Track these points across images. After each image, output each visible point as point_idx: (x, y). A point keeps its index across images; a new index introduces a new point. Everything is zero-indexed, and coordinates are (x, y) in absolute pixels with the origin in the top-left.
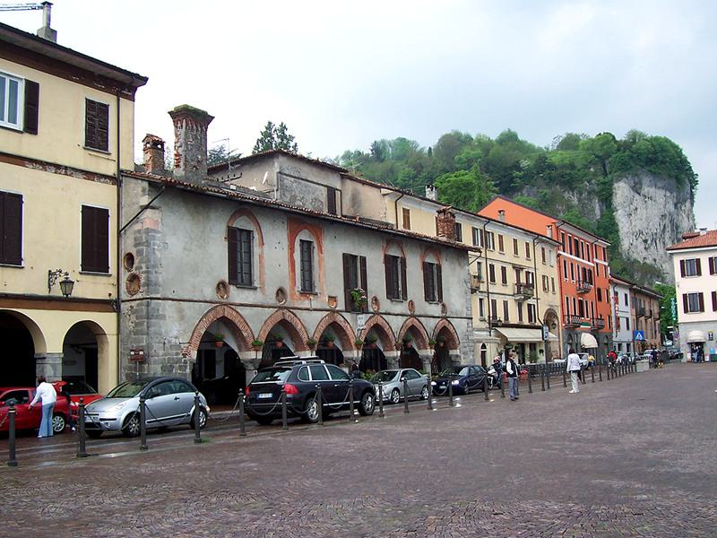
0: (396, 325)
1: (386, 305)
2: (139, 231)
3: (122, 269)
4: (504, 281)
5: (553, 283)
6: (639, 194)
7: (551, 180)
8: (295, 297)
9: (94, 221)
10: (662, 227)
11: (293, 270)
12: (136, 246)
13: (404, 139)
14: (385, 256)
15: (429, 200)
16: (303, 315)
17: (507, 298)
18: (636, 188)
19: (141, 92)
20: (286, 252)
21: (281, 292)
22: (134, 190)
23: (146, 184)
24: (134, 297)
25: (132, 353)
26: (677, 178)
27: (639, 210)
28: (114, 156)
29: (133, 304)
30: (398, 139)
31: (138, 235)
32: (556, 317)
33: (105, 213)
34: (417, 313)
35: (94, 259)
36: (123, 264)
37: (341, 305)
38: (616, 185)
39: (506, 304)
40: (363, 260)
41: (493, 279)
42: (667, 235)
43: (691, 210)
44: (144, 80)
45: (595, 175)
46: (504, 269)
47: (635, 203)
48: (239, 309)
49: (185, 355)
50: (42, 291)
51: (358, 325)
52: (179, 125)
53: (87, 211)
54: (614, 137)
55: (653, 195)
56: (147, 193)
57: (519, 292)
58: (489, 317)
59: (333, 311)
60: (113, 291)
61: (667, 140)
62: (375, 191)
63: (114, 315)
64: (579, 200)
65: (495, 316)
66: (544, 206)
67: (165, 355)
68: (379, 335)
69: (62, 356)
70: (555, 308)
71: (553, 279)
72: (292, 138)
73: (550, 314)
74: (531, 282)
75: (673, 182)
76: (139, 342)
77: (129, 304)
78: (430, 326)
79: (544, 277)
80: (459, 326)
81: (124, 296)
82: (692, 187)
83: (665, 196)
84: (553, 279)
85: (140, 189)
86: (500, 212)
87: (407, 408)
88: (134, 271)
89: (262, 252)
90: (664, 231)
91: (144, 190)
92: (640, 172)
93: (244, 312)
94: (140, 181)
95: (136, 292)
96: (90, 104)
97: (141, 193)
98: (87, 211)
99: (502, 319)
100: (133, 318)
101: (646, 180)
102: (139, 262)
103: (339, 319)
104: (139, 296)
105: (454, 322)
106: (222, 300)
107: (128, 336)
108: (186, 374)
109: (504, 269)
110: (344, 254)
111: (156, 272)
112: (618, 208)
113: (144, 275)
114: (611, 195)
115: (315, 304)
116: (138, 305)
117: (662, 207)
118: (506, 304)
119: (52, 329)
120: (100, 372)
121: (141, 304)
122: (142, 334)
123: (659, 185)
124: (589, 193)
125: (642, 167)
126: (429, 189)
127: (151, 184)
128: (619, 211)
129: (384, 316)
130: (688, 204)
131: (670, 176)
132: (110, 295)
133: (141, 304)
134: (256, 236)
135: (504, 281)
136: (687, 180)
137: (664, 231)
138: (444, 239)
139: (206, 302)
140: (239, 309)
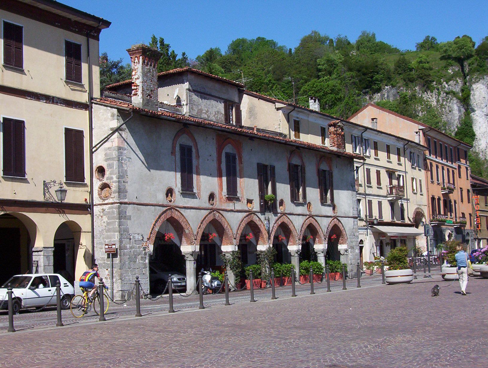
0: (297, 224)
1: (289, 207)
3: (94, 179)
4: (379, 183)
5: (421, 185)
7: (409, 81)
8: (223, 200)
9: (74, 139)
12: (106, 160)
13: (263, 38)
14: (290, 165)
15: (312, 111)
16: (187, 213)
17: (381, 199)
19: (104, 33)
21: (212, 197)
23: (115, 111)
24: (106, 202)
25: (107, 247)
28: (87, 87)
29: (104, 207)
30: (259, 39)
31: (108, 152)
32: (423, 215)
33: (81, 132)
34: (313, 213)
35: (74, 172)
36: (95, 174)
37: (256, 206)
39: (380, 203)
40: (273, 168)
41: (369, 181)
44: (107, 24)
46: (378, 173)
48: (182, 211)
49: (145, 249)
50: (40, 198)
51: (268, 222)
52: (136, 61)
53: (68, 132)
54: (470, 38)
56: (116, 117)
57: (391, 193)
58: (366, 216)
59: (251, 213)
60: (87, 196)
62: (270, 104)
63: (89, 215)
64: (438, 101)
65: (371, 215)
66: (403, 109)
67: (131, 248)
68: (284, 232)
69: (53, 249)
70: (422, 207)
71: (420, 181)
72: (168, 46)
73: (419, 215)
74: (401, 185)
76: (111, 238)
77: (100, 208)
78: (324, 225)
79: (413, 179)
80: (347, 225)
81: (97, 200)
84: (420, 181)
85: (109, 115)
86: (373, 119)
87: (60, 317)
88: (105, 181)
89: (198, 163)
91: (113, 115)
94: (109, 108)
95: (107, 197)
96: (377, 171)
97: (110, 117)
98: (68, 132)
99: (378, 218)
100: (105, 219)
102: (111, 174)
103: (255, 219)
104: (110, 201)
105: (343, 220)
106: (170, 204)
108: (146, 264)
109: (378, 173)
110: (258, 164)
111: (124, 182)
112: (476, 109)
113: (114, 184)
115: (238, 206)
116: (109, 208)
118: (380, 203)
119: (46, 229)
121: (112, 208)
126: (313, 101)
127: (119, 110)
128: (476, 112)
129: (289, 216)
132: (86, 200)
133: (112, 208)
134: (194, 150)
135: (379, 183)
138: (335, 149)
139: (160, 206)
140: (182, 211)
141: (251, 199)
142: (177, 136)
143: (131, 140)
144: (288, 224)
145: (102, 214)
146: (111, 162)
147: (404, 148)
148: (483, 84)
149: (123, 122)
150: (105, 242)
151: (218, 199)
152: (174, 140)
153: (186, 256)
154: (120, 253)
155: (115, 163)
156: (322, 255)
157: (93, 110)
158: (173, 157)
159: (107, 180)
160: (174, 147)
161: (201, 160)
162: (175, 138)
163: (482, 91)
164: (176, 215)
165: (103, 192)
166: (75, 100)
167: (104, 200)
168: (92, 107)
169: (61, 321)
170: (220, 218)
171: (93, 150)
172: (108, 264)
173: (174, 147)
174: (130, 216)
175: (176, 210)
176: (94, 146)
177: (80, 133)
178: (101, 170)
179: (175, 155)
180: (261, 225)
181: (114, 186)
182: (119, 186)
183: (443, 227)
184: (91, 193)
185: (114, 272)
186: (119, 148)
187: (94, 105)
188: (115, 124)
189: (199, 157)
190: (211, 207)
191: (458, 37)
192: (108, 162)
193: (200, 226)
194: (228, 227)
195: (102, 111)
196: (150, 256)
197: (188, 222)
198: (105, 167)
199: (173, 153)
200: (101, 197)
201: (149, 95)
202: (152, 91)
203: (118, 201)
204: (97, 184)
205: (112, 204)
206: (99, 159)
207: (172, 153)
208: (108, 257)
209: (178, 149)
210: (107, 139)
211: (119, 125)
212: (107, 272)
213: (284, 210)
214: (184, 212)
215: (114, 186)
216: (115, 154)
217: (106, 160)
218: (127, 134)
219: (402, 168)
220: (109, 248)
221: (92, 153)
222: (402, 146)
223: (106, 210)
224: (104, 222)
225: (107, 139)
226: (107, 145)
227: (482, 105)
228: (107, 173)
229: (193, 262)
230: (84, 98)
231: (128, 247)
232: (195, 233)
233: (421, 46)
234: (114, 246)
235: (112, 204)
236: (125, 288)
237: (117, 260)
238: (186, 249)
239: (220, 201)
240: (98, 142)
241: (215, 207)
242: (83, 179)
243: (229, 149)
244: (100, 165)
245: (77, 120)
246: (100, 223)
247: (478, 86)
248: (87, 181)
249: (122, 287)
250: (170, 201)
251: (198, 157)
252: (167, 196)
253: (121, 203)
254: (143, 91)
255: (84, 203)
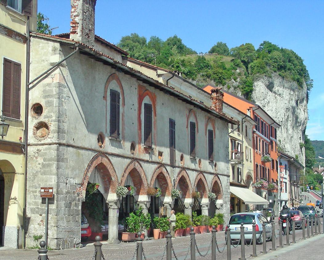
2: (49, 85)
3: (30, 117)
6: (271, 91)
10: (286, 117)
11: (140, 129)
18: (270, 87)
20: (136, 112)
22: (43, 49)
23: (57, 45)
24: (42, 142)
25: (43, 190)
26: (298, 81)
27: (270, 104)
29: (40, 147)
31: (47, 88)
36: (31, 113)
38: (255, 83)
42: (289, 123)
43: (306, 106)
45: (240, 74)
47: (268, 98)
53: (7, 62)
55: (280, 92)
56: (58, 52)
60: (22, 136)
61: (293, 52)
63: (22, 156)
75: (295, 84)
81: (31, 140)
82: (308, 89)
83: (290, 94)
85: (50, 49)
88: (42, 119)
90: (287, 120)
91: (54, 50)
92: (273, 75)
93: (114, 160)
97: (51, 51)
98: (7, 62)
101: (277, 81)
103: (164, 170)
104: (48, 141)
105: (221, 177)
107: (35, 175)
108: (79, 210)
114: (251, 91)
116: (46, 149)
117: (287, 102)
120: (154, 233)
121: (50, 149)
122: (51, 175)
123: (286, 85)
124: (235, 88)
125: (275, 71)
130: (305, 102)
131: (294, 79)
132: (21, 138)
136: (305, 84)
137: (287, 120)
141: (162, 151)
142: (108, 81)
143: (69, 78)
144: (186, 177)
145: (36, 155)
146: (50, 99)
147: (242, 121)
148: (262, 82)
149: (64, 58)
150: (39, 185)
151: (137, 149)
152: (106, 84)
153: (110, 204)
154: (57, 198)
155: (55, 101)
156: (207, 208)
157: (31, 44)
158: (105, 101)
159: (44, 118)
160: (106, 92)
161: (126, 107)
162: (107, 82)
163: (261, 87)
164: (105, 161)
165: (38, 131)
166: (15, 30)
167: (40, 141)
168: (30, 41)
169: (256, 253)
170: (139, 168)
171: (30, 86)
172: (42, 209)
173: (106, 92)
174: (67, 159)
175: (107, 158)
176: (30, 81)
177: (18, 66)
178: (38, 109)
179: (106, 100)
180: (167, 177)
181: (53, 127)
182: (59, 126)
183: (262, 190)
184: (26, 132)
185: (49, 218)
186: (60, 85)
187: (32, 39)
188: (56, 58)
189: (124, 105)
190: (132, 156)
191: (243, 45)
192: (47, 99)
193: (124, 174)
194: (145, 177)
195: (41, 45)
196: (83, 203)
197: (114, 170)
198: (43, 104)
199: (105, 98)
200: (36, 137)
201: (87, 34)
202: (90, 30)
203: (57, 142)
204: (33, 122)
205: (50, 144)
206: (35, 96)
207: (104, 97)
208: (43, 202)
209: (108, 94)
210: (47, 74)
211: (61, 60)
212: (40, 218)
213: (184, 164)
214: (112, 158)
215: (53, 127)
216: (55, 91)
217: (45, 97)
218: (66, 71)
219: (240, 138)
220: (45, 191)
221: (28, 90)
222: (241, 120)
223: (42, 151)
224: (39, 164)
225: (47, 74)
226: (48, 80)
227: (261, 98)
228: (45, 112)
229: (116, 210)
230: (22, 29)
231: (64, 192)
232: (120, 181)
233: (213, 51)
234: (51, 190)
235: (50, 144)
236: (61, 236)
237: (53, 207)
238: (112, 197)
239: (139, 151)
240: (36, 78)
241: (136, 156)
242: (18, 116)
243: (147, 100)
244: (38, 102)
245: (15, 51)
246: (35, 166)
247: (259, 83)
248: (23, 118)
249: (57, 234)
250: (101, 147)
251: (124, 104)
252: (99, 142)
253: (60, 144)
254: (83, 29)
255: (18, 141)
